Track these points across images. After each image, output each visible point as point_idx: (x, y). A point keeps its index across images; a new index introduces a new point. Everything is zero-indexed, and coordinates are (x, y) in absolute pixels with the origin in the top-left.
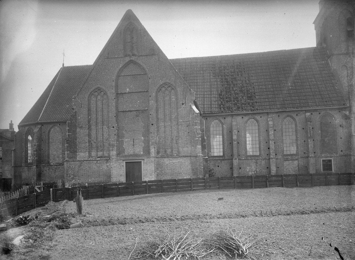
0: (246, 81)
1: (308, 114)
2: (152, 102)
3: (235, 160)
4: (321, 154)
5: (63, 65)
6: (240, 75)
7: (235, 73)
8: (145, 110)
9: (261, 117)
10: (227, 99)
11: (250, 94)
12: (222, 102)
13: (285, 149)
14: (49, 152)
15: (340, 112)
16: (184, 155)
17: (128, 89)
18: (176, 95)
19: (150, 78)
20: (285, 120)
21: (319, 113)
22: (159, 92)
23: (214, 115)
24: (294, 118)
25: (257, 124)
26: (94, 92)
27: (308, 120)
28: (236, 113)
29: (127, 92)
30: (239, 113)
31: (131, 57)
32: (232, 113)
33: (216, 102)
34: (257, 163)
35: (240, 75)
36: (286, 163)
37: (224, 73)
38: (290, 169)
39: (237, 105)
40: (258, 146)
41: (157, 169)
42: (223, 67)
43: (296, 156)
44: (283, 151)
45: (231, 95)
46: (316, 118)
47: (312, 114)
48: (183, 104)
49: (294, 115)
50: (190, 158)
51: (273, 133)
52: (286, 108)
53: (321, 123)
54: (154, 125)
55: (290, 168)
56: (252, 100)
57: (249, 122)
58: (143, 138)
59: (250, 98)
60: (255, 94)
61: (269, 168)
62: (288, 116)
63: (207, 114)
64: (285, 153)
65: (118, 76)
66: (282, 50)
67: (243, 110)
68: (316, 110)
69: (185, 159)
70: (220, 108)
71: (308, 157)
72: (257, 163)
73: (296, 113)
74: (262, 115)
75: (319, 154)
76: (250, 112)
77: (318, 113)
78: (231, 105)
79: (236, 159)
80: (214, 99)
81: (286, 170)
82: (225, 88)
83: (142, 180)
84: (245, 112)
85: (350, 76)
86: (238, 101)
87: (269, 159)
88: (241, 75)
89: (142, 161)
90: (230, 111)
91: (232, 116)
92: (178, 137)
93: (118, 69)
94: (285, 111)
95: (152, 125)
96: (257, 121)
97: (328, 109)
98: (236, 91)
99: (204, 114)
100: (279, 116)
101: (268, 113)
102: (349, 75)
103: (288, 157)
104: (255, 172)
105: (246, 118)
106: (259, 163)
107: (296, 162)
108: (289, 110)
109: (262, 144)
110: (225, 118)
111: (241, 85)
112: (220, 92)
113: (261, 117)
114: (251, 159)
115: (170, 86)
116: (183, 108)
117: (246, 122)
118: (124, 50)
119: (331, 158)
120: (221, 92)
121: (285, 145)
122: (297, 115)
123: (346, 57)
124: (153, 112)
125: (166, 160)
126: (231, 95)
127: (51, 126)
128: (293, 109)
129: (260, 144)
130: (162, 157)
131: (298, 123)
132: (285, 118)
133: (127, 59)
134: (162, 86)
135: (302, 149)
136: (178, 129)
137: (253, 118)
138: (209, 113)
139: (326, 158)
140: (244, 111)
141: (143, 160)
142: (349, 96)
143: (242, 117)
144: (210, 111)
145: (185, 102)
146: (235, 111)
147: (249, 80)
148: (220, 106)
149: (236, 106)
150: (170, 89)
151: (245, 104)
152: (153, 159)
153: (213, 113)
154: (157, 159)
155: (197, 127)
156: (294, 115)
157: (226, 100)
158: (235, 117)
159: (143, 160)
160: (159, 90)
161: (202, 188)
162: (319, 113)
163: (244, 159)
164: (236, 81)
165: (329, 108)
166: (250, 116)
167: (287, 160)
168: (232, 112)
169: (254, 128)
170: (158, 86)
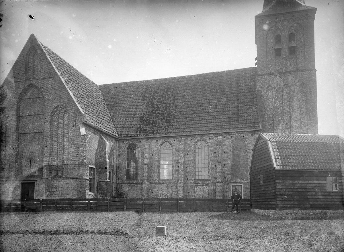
0: (170, 104)
1: (220, 137)
2: (47, 125)
3: (145, 184)
4: (231, 179)
6: (167, 99)
7: (163, 97)
8: (41, 132)
9: (175, 141)
10: (147, 122)
11: (169, 117)
12: (141, 126)
13: (197, 173)
15: (252, 135)
16: (72, 176)
17: (28, 112)
19: (46, 101)
20: (199, 144)
21: (232, 137)
22: (54, 114)
23: (135, 138)
24: (207, 142)
25: (171, 148)
27: (220, 144)
28: (150, 137)
29: (27, 115)
30: (153, 136)
31: (31, 80)
32: (147, 137)
33: (135, 125)
34: (168, 187)
35: (167, 99)
36: (197, 188)
37: (153, 97)
38: (201, 195)
39: (153, 128)
41: (48, 190)
42: (153, 91)
43: (207, 181)
44: (195, 176)
45: (151, 118)
46: (228, 142)
47: (224, 137)
48: (73, 126)
50: (76, 180)
51: (182, 157)
52: (198, 131)
54: (47, 147)
55: (201, 193)
56: (170, 123)
57: (163, 146)
58: (38, 160)
59: (168, 121)
60: (174, 117)
62: (201, 140)
63: (123, 137)
64: (197, 178)
66: (215, 72)
67: (157, 134)
68: (228, 134)
69: (72, 181)
70: (137, 132)
71: (215, 183)
72: (168, 187)
73: (208, 137)
74: (175, 139)
75: (229, 180)
76: (163, 135)
77: (230, 136)
78: (148, 128)
79: (145, 183)
80: (134, 123)
81: (196, 195)
82: (149, 111)
84: (158, 135)
85: (275, 97)
86: (156, 124)
88: (168, 98)
89: (35, 182)
90: (145, 134)
91: (147, 139)
94: (197, 135)
95: (46, 146)
96: (171, 144)
97: (240, 132)
98: (158, 115)
99: (120, 137)
100: (192, 139)
101: (181, 137)
102: (274, 96)
103: (197, 183)
104: (166, 197)
105: (160, 141)
106: (170, 187)
107: (206, 188)
108: (201, 133)
110: (140, 142)
111: (165, 108)
112: (142, 116)
113: (175, 141)
114: (163, 184)
115: (63, 109)
116: (74, 130)
117: (161, 145)
118: (26, 74)
119: (242, 184)
120: (144, 115)
121: (197, 170)
122: (210, 138)
123: (272, 77)
124: (47, 135)
125: (55, 181)
126: (151, 118)
128: (204, 132)
130: (53, 178)
131: (210, 147)
132: (198, 142)
133: (28, 83)
134: (56, 108)
135: (213, 174)
137: (167, 142)
138: (125, 137)
139: (234, 184)
140: (158, 134)
141: (36, 181)
142: (273, 119)
143: (157, 141)
144: (126, 135)
145: (75, 124)
146: (149, 135)
147: (173, 104)
148: (138, 129)
149: (152, 129)
150: (63, 111)
151: (161, 128)
152: (44, 180)
153: (128, 137)
154: (47, 181)
155: (82, 149)
156: (206, 138)
157: (146, 123)
158: (149, 140)
159: (36, 181)
160: (54, 112)
161: (45, 206)
162: (232, 137)
163: (156, 184)
164: (161, 104)
165: (242, 131)
166: (165, 140)
167: (198, 185)
168: (146, 135)
169: (168, 151)
170: (53, 108)
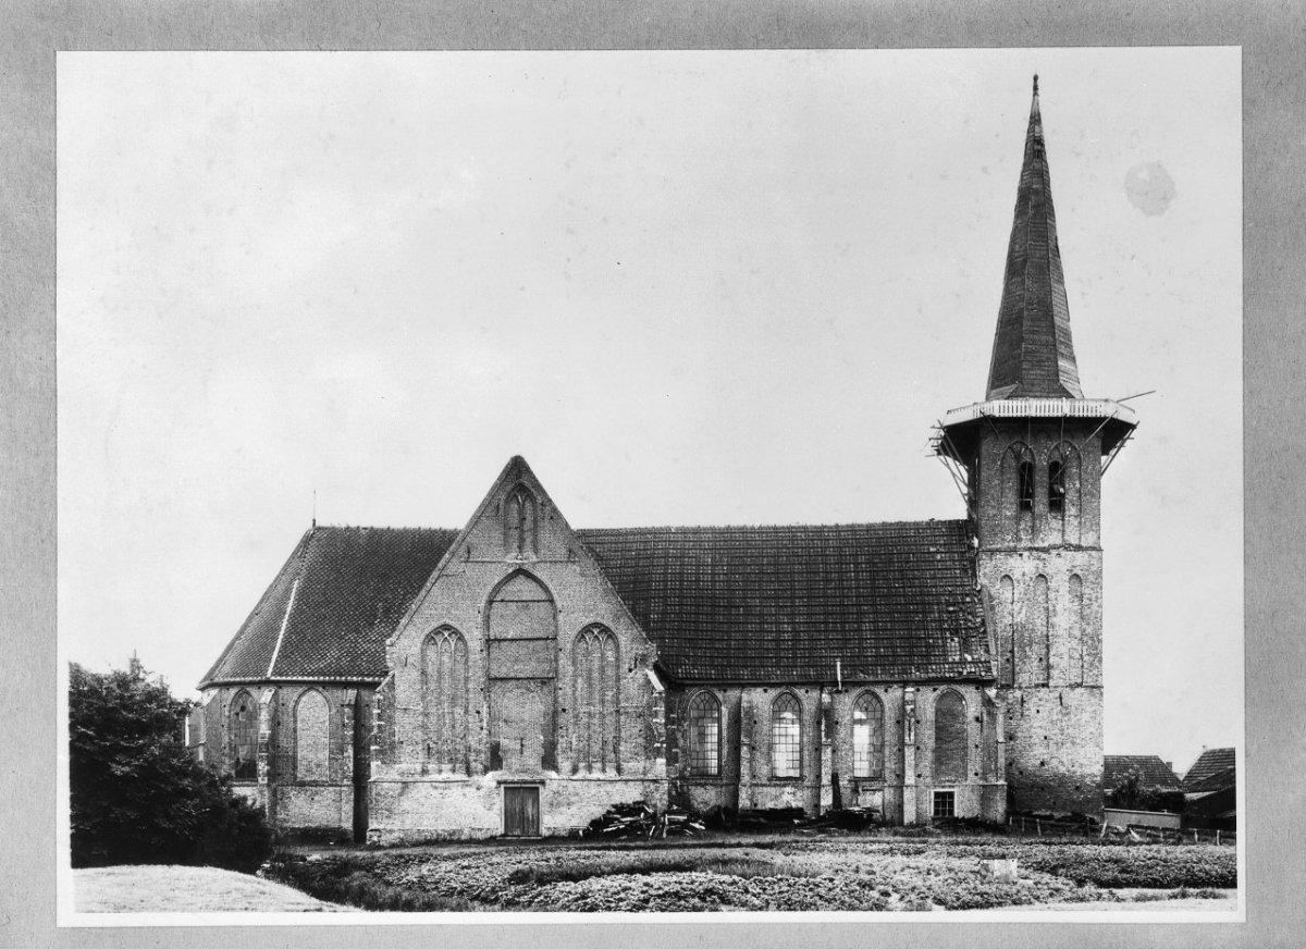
5: (314, 524)
14: (295, 753)
18: (617, 647)
22: (579, 641)
26: (436, 634)
40: (797, 756)
49: (880, 691)
53: (938, 711)
61: (900, 807)
62: (867, 692)
65: (491, 602)
83: (951, 812)
87: (819, 788)
92: (618, 740)
93: (489, 589)
109: (806, 752)
121: (857, 757)
127: (301, 690)
129: (801, 751)
136: (618, 721)
156: (880, 691)
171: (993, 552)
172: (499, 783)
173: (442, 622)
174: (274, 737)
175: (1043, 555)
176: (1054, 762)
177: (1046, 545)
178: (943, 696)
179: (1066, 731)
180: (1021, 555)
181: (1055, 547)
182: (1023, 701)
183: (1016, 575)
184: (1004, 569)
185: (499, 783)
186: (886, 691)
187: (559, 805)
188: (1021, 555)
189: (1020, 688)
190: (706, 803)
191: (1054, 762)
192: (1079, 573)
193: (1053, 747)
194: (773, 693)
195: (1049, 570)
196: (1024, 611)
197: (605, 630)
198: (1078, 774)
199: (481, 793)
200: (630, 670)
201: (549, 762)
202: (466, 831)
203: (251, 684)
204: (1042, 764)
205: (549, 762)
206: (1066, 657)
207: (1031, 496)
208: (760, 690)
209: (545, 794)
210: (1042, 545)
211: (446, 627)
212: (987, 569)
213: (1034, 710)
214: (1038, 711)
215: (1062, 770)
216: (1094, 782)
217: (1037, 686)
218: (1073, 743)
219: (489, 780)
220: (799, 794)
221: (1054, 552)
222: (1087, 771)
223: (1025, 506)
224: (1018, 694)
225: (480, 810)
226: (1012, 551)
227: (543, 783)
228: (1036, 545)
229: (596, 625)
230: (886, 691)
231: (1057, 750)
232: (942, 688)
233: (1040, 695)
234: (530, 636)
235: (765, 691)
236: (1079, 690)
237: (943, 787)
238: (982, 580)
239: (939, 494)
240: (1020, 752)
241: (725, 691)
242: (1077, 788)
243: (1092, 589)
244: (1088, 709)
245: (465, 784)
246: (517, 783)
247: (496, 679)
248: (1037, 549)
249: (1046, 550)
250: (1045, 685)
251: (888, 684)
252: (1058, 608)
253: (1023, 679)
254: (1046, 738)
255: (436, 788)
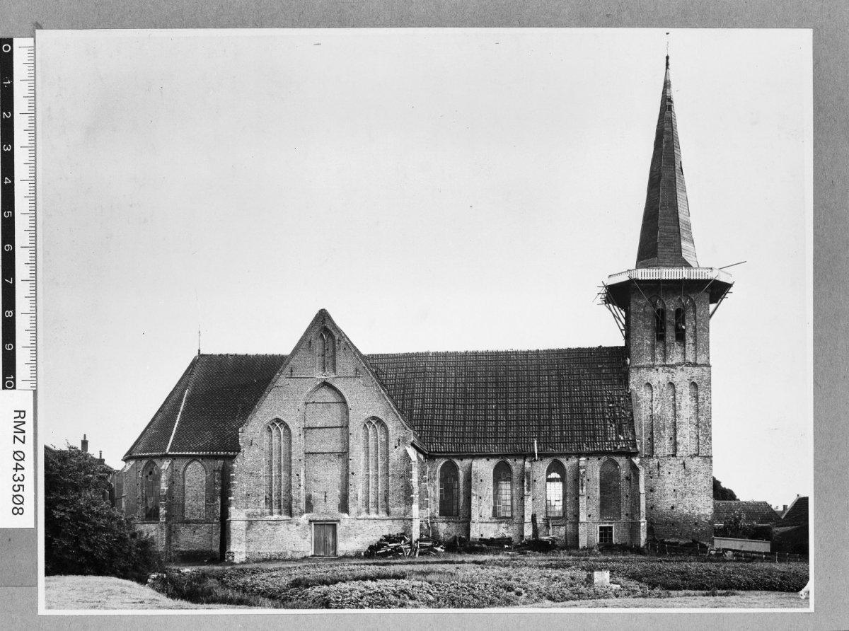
49: (563, 460)
156: (563, 460)
171: (639, 368)
172: (310, 521)
173: (275, 417)
174: (170, 491)
175: (672, 370)
176: (680, 507)
177: (674, 363)
178: (604, 464)
179: (688, 486)
180: (657, 370)
181: (679, 364)
182: (659, 466)
183: (654, 383)
184: (646, 379)
185: (310, 521)
186: (567, 460)
187: (349, 536)
188: (657, 370)
189: (657, 457)
190: (449, 534)
191: (680, 507)
192: (696, 381)
193: (679, 497)
194: (494, 462)
195: (676, 380)
196: (659, 407)
197: (379, 421)
198: (696, 514)
199: (299, 528)
200: (396, 447)
201: (344, 507)
202: (289, 553)
203: (156, 457)
204: (673, 508)
205: (344, 507)
206: (688, 437)
207: (664, 331)
208: (484, 460)
209: (340, 528)
210: (671, 363)
211: (278, 420)
212: (634, 378)
213: (666, 472)
214: (669, 473)
215: (686, 511)
216: (706, 519)
217: (669, 456)
218: (693, 494)
219: (304, 519)
220: (510, 528)
221: (679, 368)
222: (703, 513)
223: (660, 336)
224: (656, 461)
225: (299, 539)
226: (651, 367)
227: (339, 521)
228: (667, 363)
229: (374, 418)
230: (567, 460)
231: (683, 498)
232: (604, 458)
233: (671, 462)
234: (331, 425)
235: (488, 460)
236: (696, 459)
237: (605, 523)
238: (632, 387)
239: (604, 329)
240: (658, 500)
241: (462, 460)
242: (696, 524)
243: (705, 392)
244: (703, 471)
245: (290, 522)
246: (331, 521)
247: (309, 453)
248: (668, 366)
249: (672, 366)
250: (674, 455)
251: (568, 455)
252: (683, 404)
253: (659, 451)
254: (674, 490)
255: (270, 524)
